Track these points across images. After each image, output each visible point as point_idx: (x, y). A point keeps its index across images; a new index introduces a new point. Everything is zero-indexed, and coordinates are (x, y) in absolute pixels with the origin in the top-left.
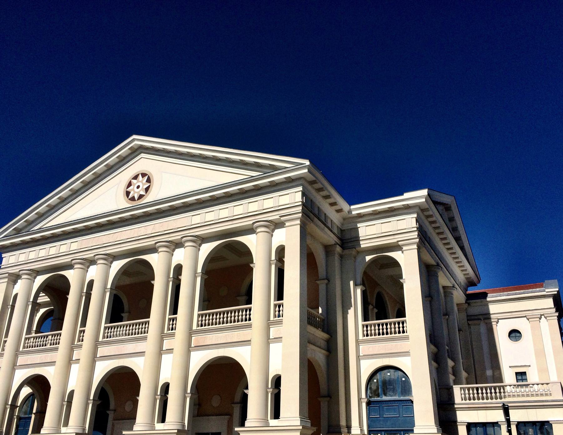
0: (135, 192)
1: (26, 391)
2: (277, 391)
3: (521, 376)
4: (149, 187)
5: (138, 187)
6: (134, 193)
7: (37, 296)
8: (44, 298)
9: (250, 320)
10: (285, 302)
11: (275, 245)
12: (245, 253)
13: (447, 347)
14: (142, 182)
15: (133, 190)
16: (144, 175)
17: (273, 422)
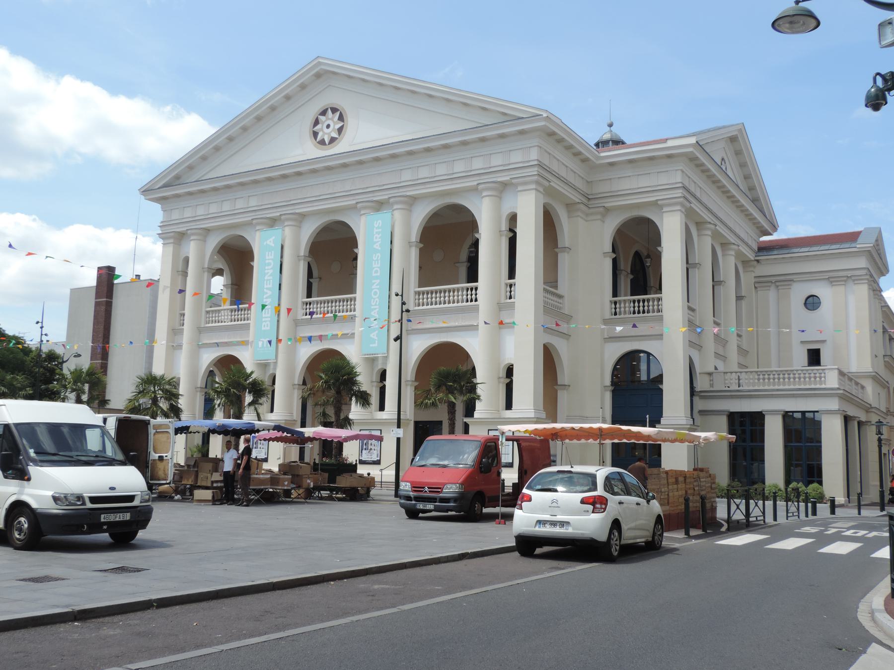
0: (325, 134)
2: (508, 380)
4: (342, 127)
9: (476, 300)
11: (506, 211)
13: (8, 377)
14: (325, 134)
16: (334, 110)
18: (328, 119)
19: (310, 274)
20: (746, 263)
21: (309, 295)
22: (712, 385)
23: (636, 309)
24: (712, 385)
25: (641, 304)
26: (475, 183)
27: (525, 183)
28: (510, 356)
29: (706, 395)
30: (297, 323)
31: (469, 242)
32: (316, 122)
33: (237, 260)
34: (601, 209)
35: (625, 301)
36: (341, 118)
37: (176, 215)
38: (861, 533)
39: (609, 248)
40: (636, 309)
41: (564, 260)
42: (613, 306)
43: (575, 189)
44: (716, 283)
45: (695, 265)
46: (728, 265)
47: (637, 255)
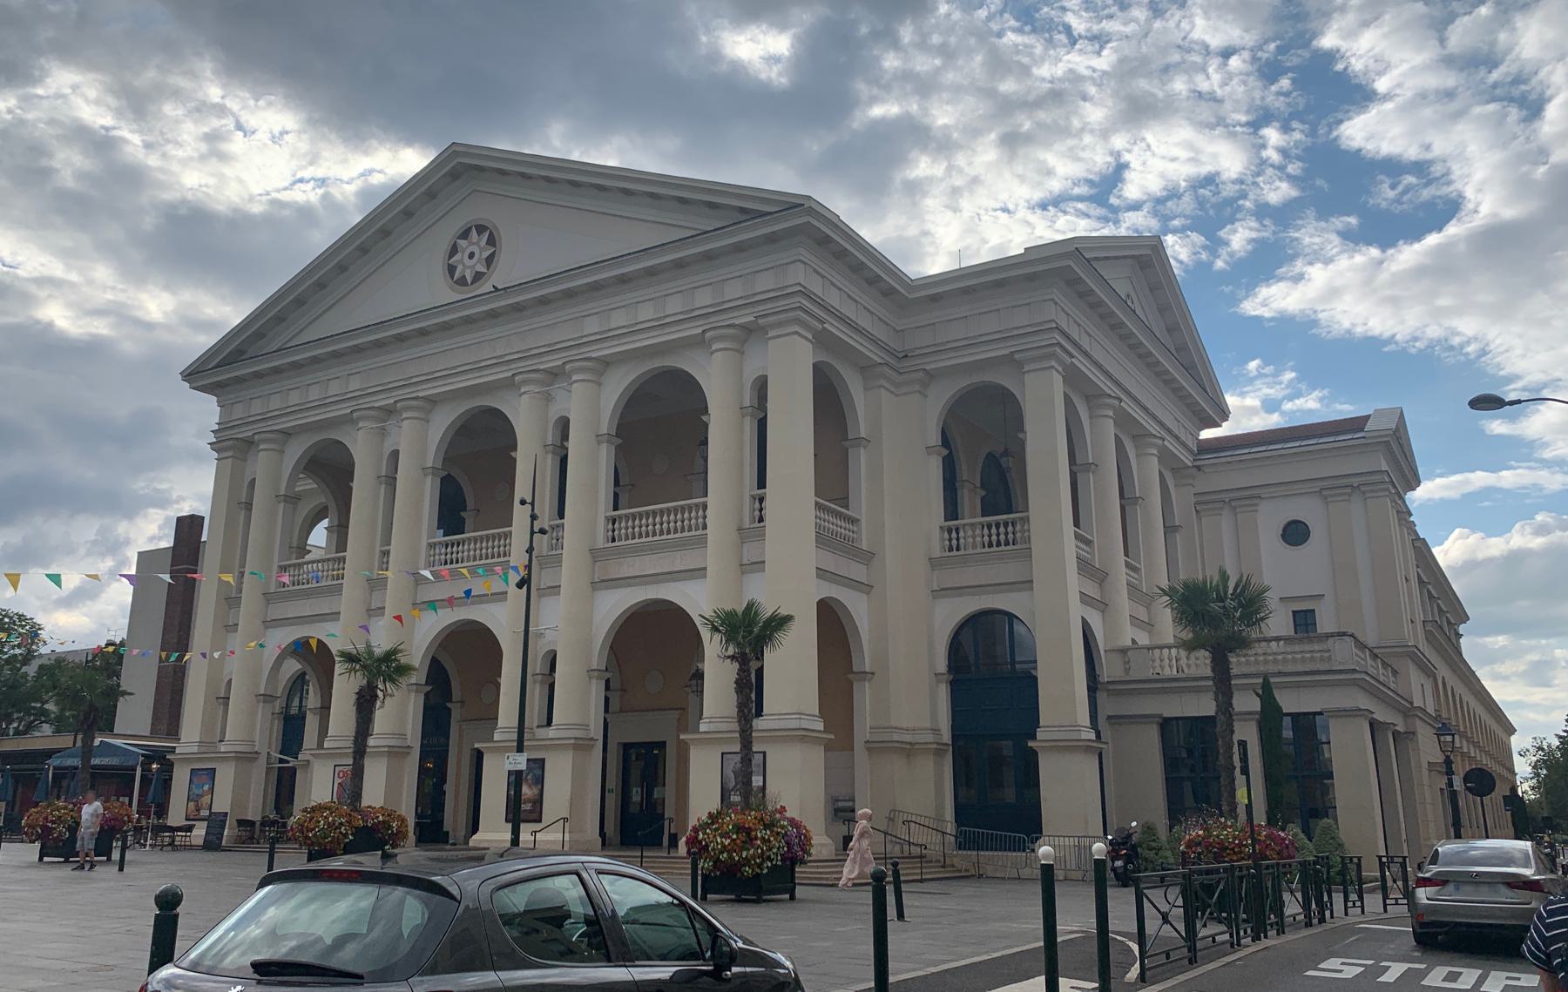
0: (466, 267)
1: (293, 666)
3: (1304, 621)
5: (471, 256)
7: (293, 479)
8: (307, 484)
9: (705, 527)
10: (769, 491)
14: (466, 267)
16: (481, 229)
20: (1178, 469)
22: (1127, 671)
23: (994, 538)
24: (1127, 671)
25: (1002, 529)
26: (700, 330)
27: (780, 324)
29: (1121, 689)
32: (454, 250)
33: (330, 471)
35: (972, 525)
36: (492, 241)
37: (239, 412)
38: (1508, 478)
39: (934, 438)
40: (994, 538)
41: (861, 461)
42: (946, 536)
43: (874, 341)
44: (1127, 500)
45: (1087, 467)
46: (1147, 473)
47: (990, 457)
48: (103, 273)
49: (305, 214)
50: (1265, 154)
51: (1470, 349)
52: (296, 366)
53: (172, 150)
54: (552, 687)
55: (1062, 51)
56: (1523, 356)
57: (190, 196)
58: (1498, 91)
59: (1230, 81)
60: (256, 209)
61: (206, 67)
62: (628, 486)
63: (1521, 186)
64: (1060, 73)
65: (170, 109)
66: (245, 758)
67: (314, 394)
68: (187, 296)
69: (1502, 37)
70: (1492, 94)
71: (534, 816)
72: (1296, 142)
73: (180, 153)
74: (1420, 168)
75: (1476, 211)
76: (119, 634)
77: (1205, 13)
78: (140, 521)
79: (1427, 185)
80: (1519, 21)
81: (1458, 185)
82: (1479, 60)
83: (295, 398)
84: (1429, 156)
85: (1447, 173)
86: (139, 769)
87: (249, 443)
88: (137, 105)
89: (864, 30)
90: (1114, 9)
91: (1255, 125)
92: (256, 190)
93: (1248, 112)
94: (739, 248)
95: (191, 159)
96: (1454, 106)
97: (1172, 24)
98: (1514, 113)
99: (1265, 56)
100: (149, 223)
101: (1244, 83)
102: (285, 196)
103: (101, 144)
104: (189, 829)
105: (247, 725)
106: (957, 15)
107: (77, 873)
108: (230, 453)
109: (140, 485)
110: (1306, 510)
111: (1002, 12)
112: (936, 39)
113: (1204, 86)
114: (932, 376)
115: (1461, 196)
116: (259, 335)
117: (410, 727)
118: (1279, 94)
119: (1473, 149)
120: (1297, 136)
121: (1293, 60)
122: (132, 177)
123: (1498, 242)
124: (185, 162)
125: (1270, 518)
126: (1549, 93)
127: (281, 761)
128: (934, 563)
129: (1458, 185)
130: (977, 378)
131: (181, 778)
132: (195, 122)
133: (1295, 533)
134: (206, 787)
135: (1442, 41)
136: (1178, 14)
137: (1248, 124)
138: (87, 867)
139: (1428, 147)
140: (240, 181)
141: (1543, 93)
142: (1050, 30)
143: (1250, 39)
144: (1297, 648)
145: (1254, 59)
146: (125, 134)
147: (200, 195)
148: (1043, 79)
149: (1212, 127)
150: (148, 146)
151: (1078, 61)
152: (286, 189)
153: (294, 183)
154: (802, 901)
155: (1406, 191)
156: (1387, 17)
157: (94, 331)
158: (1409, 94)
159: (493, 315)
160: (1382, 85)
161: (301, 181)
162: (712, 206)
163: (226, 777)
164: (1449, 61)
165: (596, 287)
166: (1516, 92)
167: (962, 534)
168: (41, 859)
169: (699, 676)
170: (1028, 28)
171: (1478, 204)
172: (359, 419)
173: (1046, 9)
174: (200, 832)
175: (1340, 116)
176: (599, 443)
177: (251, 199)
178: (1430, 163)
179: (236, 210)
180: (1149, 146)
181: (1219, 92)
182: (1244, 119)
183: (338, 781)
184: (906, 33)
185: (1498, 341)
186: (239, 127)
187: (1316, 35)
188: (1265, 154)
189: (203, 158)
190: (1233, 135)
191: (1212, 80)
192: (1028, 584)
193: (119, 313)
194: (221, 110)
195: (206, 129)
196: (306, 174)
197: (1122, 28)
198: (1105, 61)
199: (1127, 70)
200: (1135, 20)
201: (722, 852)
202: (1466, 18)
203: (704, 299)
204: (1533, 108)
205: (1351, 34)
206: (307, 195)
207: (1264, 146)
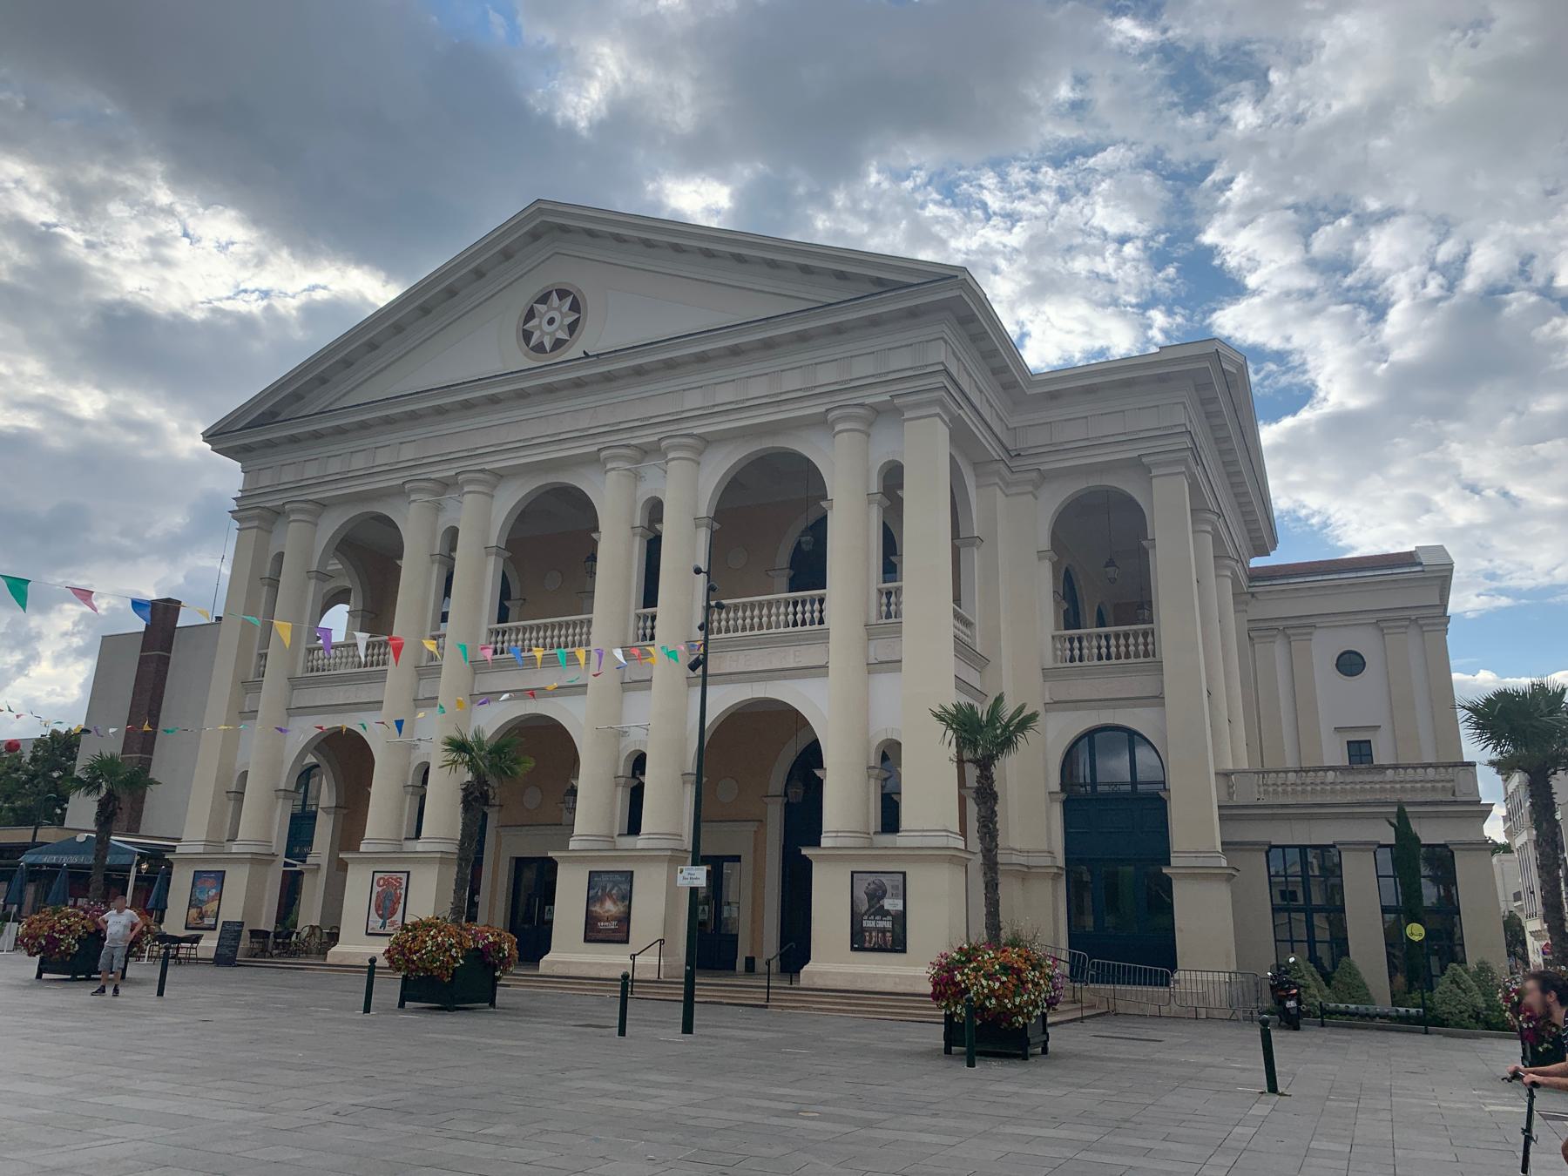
0: (545, 333)
5: (551, 321)
6: (542, 336)
7: (323, 560)
9: (821, 622)
11: (444, 523)
12: (808, 479)
14: (545, 333)
15: (563, 316)
16: (562, 294)
17: (887, 839)
18: (551, 309)
19: (505, 593)
21: (503, 618)
22: (1230, 795)
25: (1122, 641)
27: (917, 405)
28: (885, 725)
30: (477, 667)
31: (801, 524)
32: (530, 315)
34: (1034, 474)
36: (575, 307)
48: (32, 366)
49: (246, 324)
50: (1150, 333)
51: (1314, 521)
52: (340, 431)
53: (113, 251)
54: (423, 798)
55: (977, 225)
56: (1358, 530)
57: (129, 297)
58: (1351, 294)
59: (1125, 268)
60: (197, 315)
61: (156, 167)
62: (723, 578)
63: (1364, 380)
64: (974, 247)
65: (117, 209)
66: (259, 860)
67: (358, 462)
68: (119, 396)
69: (1358, 246)
70: (1345, 296)
71: (618, 936)
72: (1178, 326)
73: (123, 255)
74: (1280, 357)
75: (1325, 399)
76: (76, 722)
77: (1105, 201)
78: (53, 616)
79: (1284, 373)
80: (1373, 234)
81: (1312, 375)
82: (1338, 265)
83: (335, 467)
84: (1289, 347)
85: (1304, 364)
86: (134, 870)
87: (278, 513)
88: (82, 201)
89: (801, 190)
90: (1026, 191)
91: (1144, 307)
92: (198, 298)
93: (1138, 295)
94: (874, 322)
95: (133, 262)
96: (1315, 303)
97: (1075, 210)
98: (1363, 315)
99: (1155, 245)
100: (84, 321)
101: (1137, 269)
102: (227, 305)
103: (41, 239)
104: (197, 939)
105: (261, 823)
106: (885, 185)
107: (98, 998)
108: (256, 523)
109: (60, 579)
110: (1361, 641)
111: (926, 185)
112: (866, 205)
113: (1101, 267)
114: (1045, 477)
115: (1314, 384)
116: (297, 397)
117: (275, 834)
118: (1166, 280)
119: (1327, 344)
120: (1179, 319)
121: (1179, 252)
122: (72, 274)
123: (1343, 425)
124: (128, 264)
125: (1325, 648)
126: (1393, 298)
127: (286, 864)
128: (1047, 673)
129: (1312, 375)
130: (1094, 482)
131: (181, 881)
132: (143, 225)
133: (1350, 664)
134: (213, 892)
135: (1307, 246)
136: (1082, 201)
137: (1137, 306)
138: (109, 991)
139: (1288, 339)
140: (182, 287)
141: (1387, 300)
142: (968, 206)
143: (1144, 229)
144: (1349, 779)
145: (1146, 248)
146: (67, 232)
147: (139, 299)
148: (959, 251)
149: (1103, 305)
150: (90, 245)
151: (992, 235)
152: (229, 298)
153: (238, 293)
154: (1057, 1056)
155: (1267, 377)
156: (1261, 220)
157: (19, 423)
158: (1275, 292)
159: (578, 384)
160: (1252, 281)
161: (245, 291)
162: (841, 276)
163: (237, 882)
164: (1312, 264)
165: (702, 358)
166: (1366, 296)
167: (1085, 643)
168: (39, 976)
169: (573, 792)
170: (949, 201)
171: (1328, 393)
172: (413, 491)
173: (965, 186)
174: (209, 944)
175: (1214, 305)
176: (697, 526)
177: (193, 306)
178: (1290, 353)
179: (176, 315)
180: (1048, 320)
181: (1114, 276)
182: (1134, 300)
183: (377, 889)
184: (840, 199)
185: (1338, 515)
186: (186, 235)
187: (1200, 230)
188: (1150, 333)
189: (145, 262)
190: (1124, 314)
191: (1106, 265)
192: (1158, 699)
193: (47, 407)
194: (169, 212)
195: (151, 233)
196: (250, 286)
197: (1033, 210)
198: (1017, 237)
199: (1039, 246)
200: (1044, 203)
201: (988, 997)
202: (1329, 228)
203: (827, 376)
204: (1379, 311)
205: (1227, 234)
206: (254, 306)
207: (1150, 327)
